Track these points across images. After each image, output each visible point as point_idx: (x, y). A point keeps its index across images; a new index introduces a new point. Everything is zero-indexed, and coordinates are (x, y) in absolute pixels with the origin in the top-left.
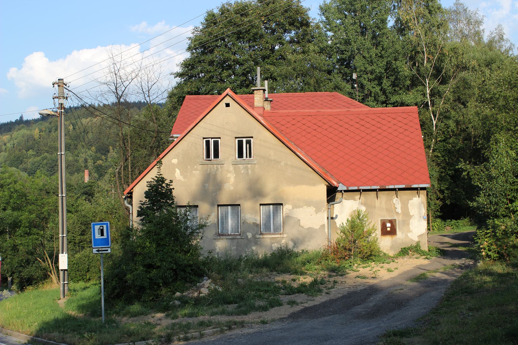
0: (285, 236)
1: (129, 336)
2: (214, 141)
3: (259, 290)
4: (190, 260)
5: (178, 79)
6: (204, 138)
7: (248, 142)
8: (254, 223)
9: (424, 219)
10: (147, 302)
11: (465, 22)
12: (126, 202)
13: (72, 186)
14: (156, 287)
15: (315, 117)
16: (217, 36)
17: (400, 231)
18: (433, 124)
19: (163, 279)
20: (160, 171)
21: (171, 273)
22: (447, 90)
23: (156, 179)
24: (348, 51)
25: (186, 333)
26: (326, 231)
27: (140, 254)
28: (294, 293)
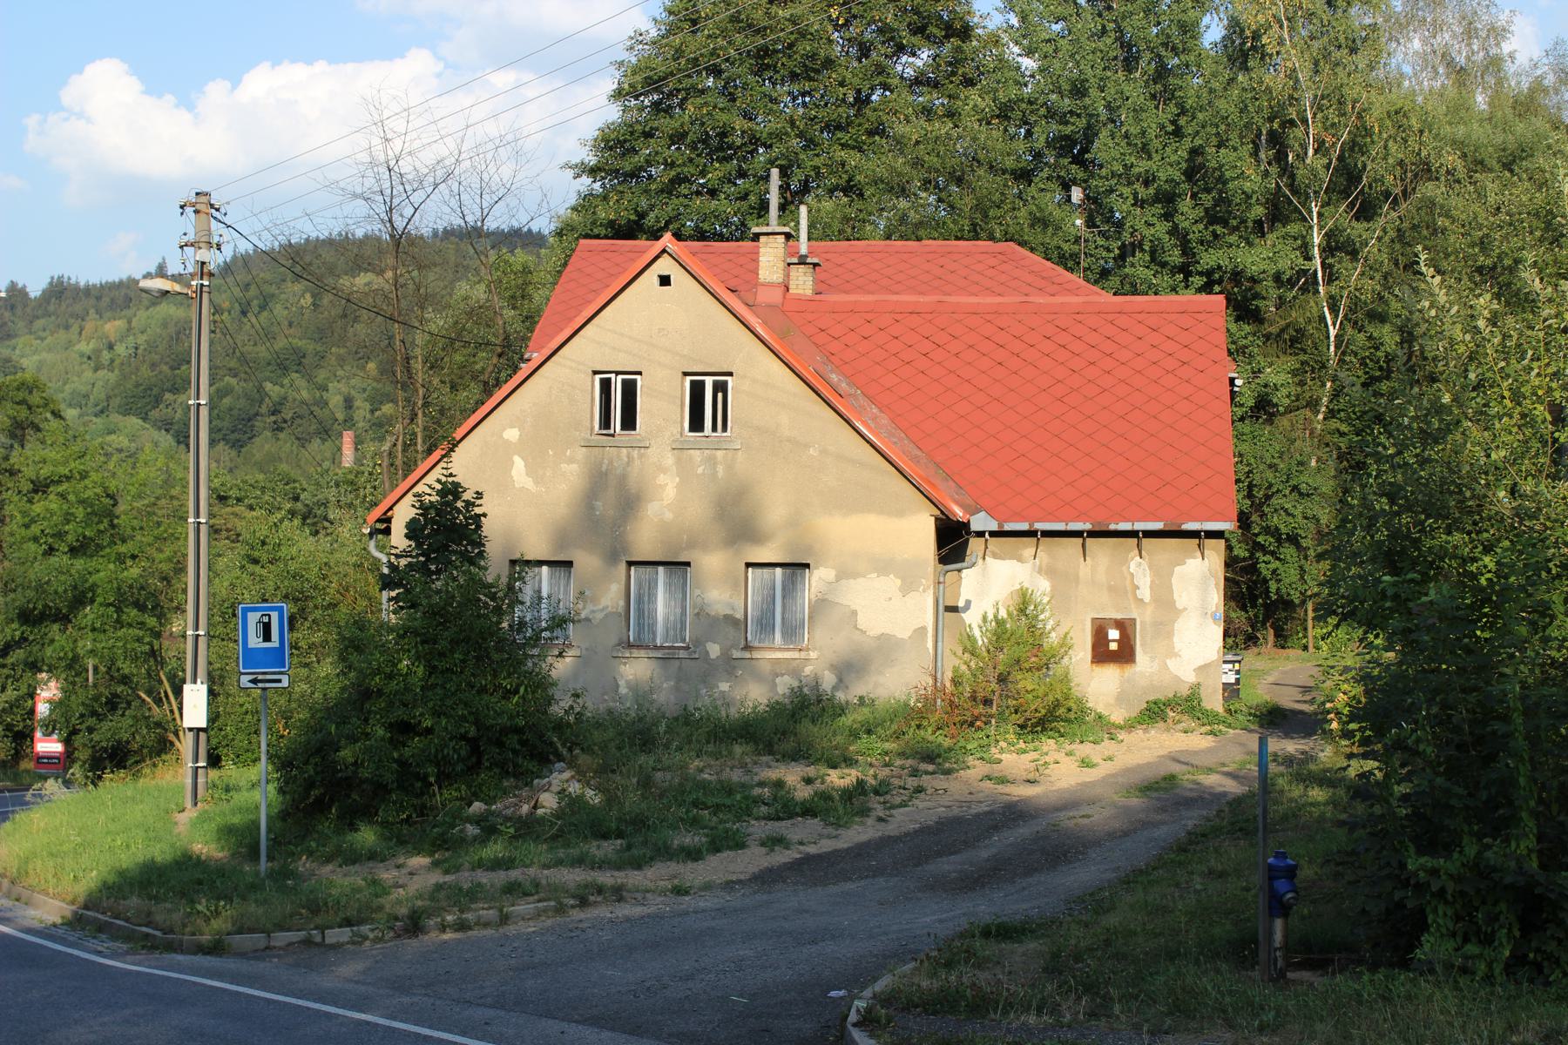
0: (813, 655)
1: (312, 912)
2: (623, 381)
3: (695, 804)
4: (518, 715)
5: (586, 180)
6: (595, 373)
7: (720, 388)
8: (727, 617)
9: (1215, 619)
10: (393, 824)
11: (1459, 30)
12: (372, 544)
13: (295, 481)
14: (419, 784)
15: (929, 317)
16: (696, 59)
17: (1145, 653)
18: (1328, 337)
19: (437, 765)
20: (450, 465)
21: (461, 747)
22: (1373, 237)
23: (439, 487)
24: (1079, 116)
25: (462, 911)
26: (930, 644)
27: (380, 693)
28: (791, 815)
